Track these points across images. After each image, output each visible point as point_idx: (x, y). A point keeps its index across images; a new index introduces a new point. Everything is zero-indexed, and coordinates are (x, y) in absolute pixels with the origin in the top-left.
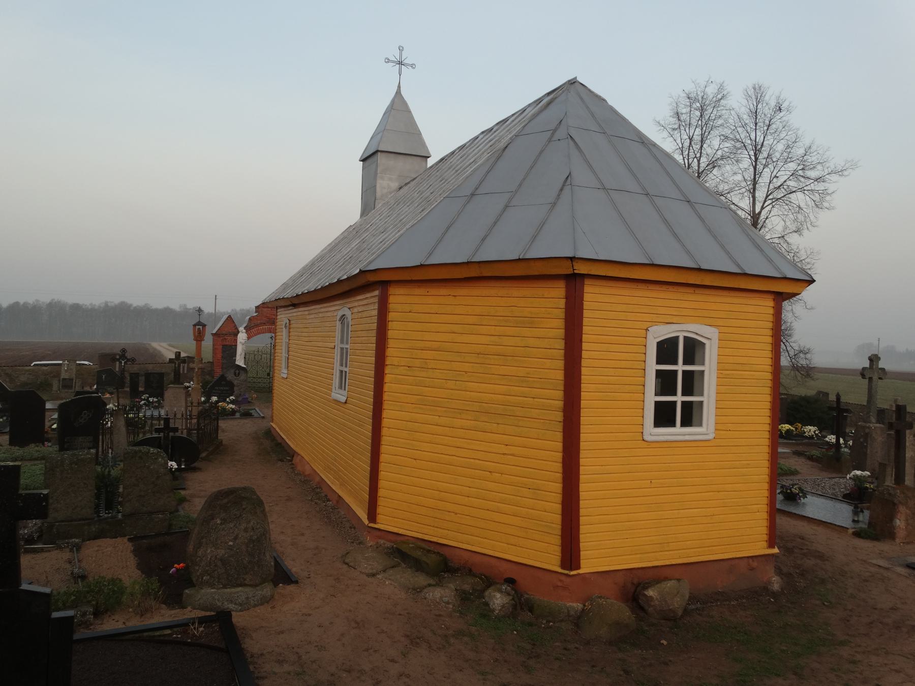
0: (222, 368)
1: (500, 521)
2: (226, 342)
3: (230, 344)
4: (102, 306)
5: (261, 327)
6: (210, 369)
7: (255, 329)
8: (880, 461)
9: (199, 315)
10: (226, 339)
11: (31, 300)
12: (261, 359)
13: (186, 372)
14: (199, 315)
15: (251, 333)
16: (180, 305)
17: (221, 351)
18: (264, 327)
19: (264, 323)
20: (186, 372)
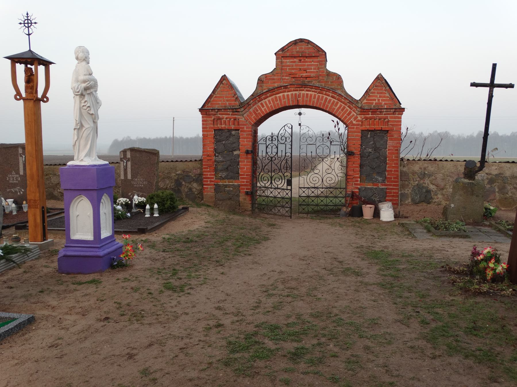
0: (216, 170)
1: (67, 188)
2: (221, 124)
3: (227, 127)
4: (318, 134)
5: (281, 95)
6: (199, 171)
7: (270, 98)
8: (79, 56)
9: (29, 35)
10: (219, 119)
11: (163, 136)
12: (277, 153)
13: (129, 177)
14: (29, 35)
15: (263, 106)
16: (495, 132)
17: (213, 140)
18: (286, 94)
19: (285, 87)
20: (129, 177)
